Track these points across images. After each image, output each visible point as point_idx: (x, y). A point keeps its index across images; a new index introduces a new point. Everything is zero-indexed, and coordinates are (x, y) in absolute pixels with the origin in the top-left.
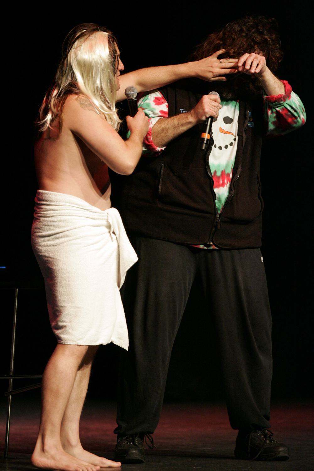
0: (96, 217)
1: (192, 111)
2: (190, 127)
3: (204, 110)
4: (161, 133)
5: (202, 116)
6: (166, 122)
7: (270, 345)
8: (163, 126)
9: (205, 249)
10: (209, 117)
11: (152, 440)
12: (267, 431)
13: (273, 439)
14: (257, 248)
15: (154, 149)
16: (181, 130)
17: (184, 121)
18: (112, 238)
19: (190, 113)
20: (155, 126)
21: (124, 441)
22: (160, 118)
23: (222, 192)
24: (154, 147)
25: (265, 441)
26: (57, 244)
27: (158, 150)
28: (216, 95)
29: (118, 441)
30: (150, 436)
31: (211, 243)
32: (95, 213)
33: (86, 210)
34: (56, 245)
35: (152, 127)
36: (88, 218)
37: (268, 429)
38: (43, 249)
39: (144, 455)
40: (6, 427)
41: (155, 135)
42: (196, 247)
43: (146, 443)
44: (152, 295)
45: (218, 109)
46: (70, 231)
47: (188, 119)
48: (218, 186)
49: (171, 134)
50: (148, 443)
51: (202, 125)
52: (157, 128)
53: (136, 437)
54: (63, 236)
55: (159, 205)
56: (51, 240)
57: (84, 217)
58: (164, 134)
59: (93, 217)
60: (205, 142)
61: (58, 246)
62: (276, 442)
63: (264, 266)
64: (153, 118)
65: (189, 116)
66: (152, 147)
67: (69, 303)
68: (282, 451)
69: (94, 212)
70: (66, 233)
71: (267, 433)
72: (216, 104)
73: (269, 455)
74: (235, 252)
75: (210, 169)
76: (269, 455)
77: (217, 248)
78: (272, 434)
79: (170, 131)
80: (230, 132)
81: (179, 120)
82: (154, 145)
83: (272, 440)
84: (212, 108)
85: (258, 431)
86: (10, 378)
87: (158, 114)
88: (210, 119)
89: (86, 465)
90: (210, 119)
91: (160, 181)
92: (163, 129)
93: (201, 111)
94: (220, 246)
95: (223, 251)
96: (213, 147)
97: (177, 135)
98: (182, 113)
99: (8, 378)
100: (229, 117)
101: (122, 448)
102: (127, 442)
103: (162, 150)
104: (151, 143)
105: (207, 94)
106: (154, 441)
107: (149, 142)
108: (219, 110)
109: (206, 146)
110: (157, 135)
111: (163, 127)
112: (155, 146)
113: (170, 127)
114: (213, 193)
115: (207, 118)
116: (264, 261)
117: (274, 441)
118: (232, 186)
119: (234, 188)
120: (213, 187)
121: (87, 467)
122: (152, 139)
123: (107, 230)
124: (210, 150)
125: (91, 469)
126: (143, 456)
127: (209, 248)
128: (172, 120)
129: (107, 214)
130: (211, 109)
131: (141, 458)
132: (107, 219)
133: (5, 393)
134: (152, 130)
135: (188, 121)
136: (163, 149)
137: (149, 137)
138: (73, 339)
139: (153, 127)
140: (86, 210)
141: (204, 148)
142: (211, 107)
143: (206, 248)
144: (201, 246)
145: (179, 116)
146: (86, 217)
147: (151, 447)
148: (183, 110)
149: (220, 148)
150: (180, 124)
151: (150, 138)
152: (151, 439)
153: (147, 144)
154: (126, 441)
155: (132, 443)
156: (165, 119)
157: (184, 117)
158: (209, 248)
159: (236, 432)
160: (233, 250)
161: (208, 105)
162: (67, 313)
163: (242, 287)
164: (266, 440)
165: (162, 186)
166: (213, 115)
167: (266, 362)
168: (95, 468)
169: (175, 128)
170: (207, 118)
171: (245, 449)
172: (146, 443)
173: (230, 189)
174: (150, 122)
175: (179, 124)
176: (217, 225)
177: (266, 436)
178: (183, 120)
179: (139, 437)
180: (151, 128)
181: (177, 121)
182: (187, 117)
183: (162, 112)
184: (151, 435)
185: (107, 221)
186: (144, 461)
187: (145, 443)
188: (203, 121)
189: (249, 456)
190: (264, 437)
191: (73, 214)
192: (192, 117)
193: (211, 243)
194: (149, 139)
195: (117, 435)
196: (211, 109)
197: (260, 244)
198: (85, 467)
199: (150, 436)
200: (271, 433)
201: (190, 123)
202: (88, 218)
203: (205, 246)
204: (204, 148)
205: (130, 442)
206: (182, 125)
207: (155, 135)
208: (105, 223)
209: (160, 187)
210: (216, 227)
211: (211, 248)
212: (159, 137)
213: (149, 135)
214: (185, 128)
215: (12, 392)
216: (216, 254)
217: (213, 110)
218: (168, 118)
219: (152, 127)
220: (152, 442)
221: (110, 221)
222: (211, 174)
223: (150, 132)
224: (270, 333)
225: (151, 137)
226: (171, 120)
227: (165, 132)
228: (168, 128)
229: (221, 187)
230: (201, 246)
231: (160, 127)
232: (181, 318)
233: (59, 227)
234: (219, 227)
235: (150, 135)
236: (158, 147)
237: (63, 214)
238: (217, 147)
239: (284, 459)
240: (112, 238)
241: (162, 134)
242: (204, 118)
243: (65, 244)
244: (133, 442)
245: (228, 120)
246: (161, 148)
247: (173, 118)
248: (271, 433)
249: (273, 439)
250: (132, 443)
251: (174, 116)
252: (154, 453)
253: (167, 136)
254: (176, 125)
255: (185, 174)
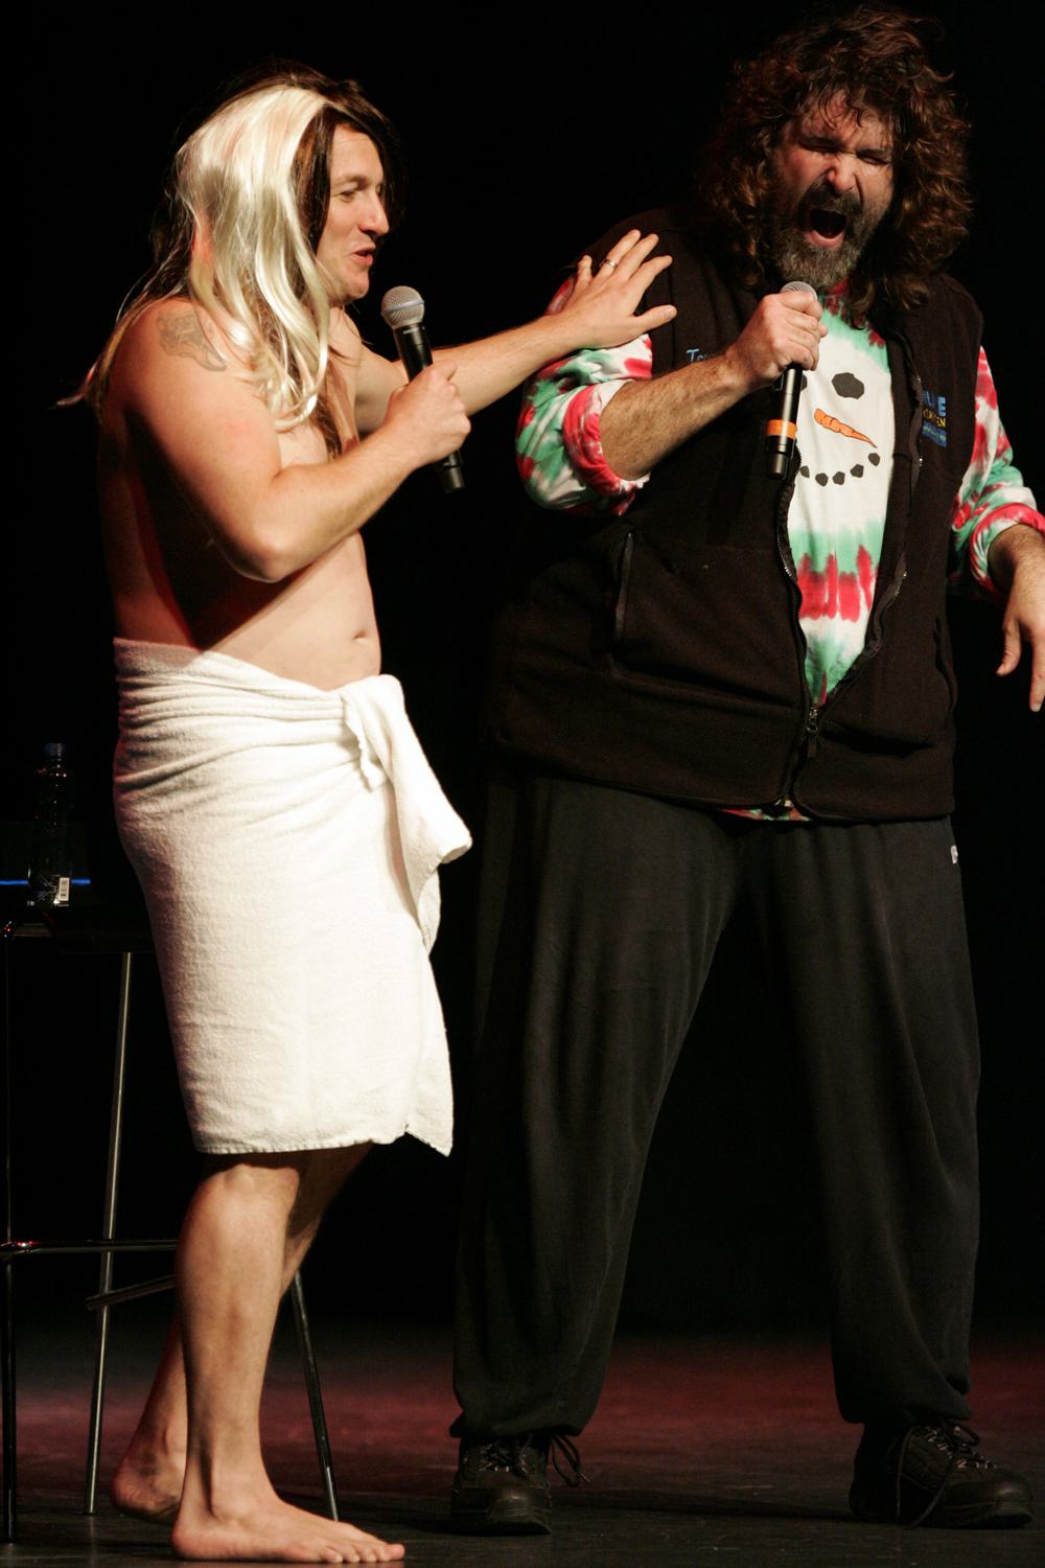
0: (296, 714)
1: (730, 352)
2: (728, 406)
3: (770, 343)
4: (631, 431)
5: (765, 364)
6: (646, 392)
7: (972, 1142)
8: (636, 405)
9: (768, 821)
10: (790, 366)
11: (574, 1457)
12: (957, 1429)
13: (977, 1455)
14: (941, 818)
15: (611, 484)
16: (696, 415)
17: (708, 389)
18: (367, 786)
19: (725, 359)
20: (612, 406)
21: (483, 1461)
22: (624, 382)
23: (839, 637)
24: (610, 478)
25: (953, 1463)
26: (163, 812)
27: (623, 490)
28: (805, 291)
29: (461, 1459)
30: (567, 1441)
31: (788, 803)
32: (290, 701)
33: (253, 691)
34: (160, 819)
35: (599, 412)
36: (265, 717)
37: (962, 1422)
38: (147, 825)
39: (548, 1508)
40: (89, 1413)
41: (612, 437)
42: (737, 816)
43: (557, 1468)
44: (587, 972)
45: (815, 337)
46: (200, 768)
47: (718, 379)
48: (819, 610)
49: (666, 431)
50: (561, 1467)
51: (767, 399)
52: (619, 412)
53: (522, 1445)
54: (180, 785)
55: (617, 674)
56: (145, 799)
57: (249, 715)
58: (643, 432)
59: (286, 714)
60: (782, 448)
61: (165, 820)
62: (990, 1465)
63: (959, 877)
64: (602, 382)
65: (722, 369)
66: (602, 477)
67: (207, 1015)
68: (1009, 1497)
69: (284, 698)
70: (187, 775)
71: (958, 1435)
72: (807, 321)
73: (964, 1509)
74: (867, 833)
75: (789, 552)
76: (964, 1509)
77: (806, 819)
78: (977, 1438)
79: (661, 420)
80: (854, 431)
81: (686, 383)
82: (610, 472)
83: (976, 1458)
84: (798, 334)
85: (928, 1428)
86: (104, 1248)
87: (618, 372)
88: (792, 373)
89: (357, 1541)
90: (792, 373)
91: (618, 593)
92: (637, 417)
93: (760, 347)
94: (812, 811)
95: (827, 831)
96: (799, 478)
97: (685, 434)
98: (695, 361)
99: (99, 1249)
100: (852, 376)
101: (477, 1487)
102: (491, 1464)
103: (635, 489)
104: (600, 466)
105: (777, 291)
106: (583, 1460)
107: (591, 461)
108: (819, 342)
109: (785, 460)
110: (618, 438)
111: (638, 408)
112: (613, 475)
113: (660, 407)
114: (799, 636)
115: (784, 371)
116: (959, 857)
117: (982, 1462)
118: (876, 623)
119: (883, 631)
120: (797, 614)
121: (360, 1546)
122: (601, 451)
123: (345, 755)
124: (789, 488)
125: (375, 1553)
126: (545, 1510)
127: (781, 818)
128: (665, 385)
129: (342, 700)
130: (795, 337)
131: (539, 1518)
132: (343, 718)
133: (88, 1299)
134: (600, 420)
135: (719, 384)
136: (640, 483)
137: (592, 444)
138: (233, 1137)
139: (604, 411)
140: (253, 691)
141: (778, 470)
142: (794, 332)
143: (767, 818)
144: (754, 812)
145: (687, 370)
146: (258, 716)
147: (573, 1479)
148: (696, 354)
149: (822, 479)
150: (693, 396)
151: (597, 449)
152: (570, 1451)
153: (587, 469)
154: (489, 1460)
155: (507, 1469)
156: (641, 384)
157: (706, 372)
158: (781, 818)
159: (860, 1428)
160: (859, 827)
161: (784, 328)
162: (203, 1046)
163: (888, 946)
164: (954, 1459)
165: (626, 610)
166: (800, 359)
167: (962, 1195)
168: (387, 1551)
169: (675, 410)
170: (784, 371)
171: (888, 1490)
172: (557, 1468)
173: (870, 635)
174: (595, 395)
175: (688, 395)
176: (806, 744)
177: (953, 1443)
178: (703, 383)
179: (531, 1445)
180: (597, 415)
181: (682, 385)
182: (715, 373)
183: (633, 364)
184: (571, 1439)
185: (344, 726)
186: (547, 1527)
187: (550, 1467)
188: (769, 380)
189: (898, 1511)
190: (949, 1449)
191: (207, 710)
192: (732, 371)
193: (788, 803)
194: (592, 453)
195: (457, 1441)
196: (795, 337)
197: (950, 805)
198: (354, 1547)
199: (567, 1441)
200: (973, 1435)
201: (726, 390)
202: (265, 717)
203: (765, 812)
204: (778, 470)
205: (503, 1466)
206: (700, 399)
207: (612, 437)
208: (335, 730)
209: (620, 614)
210: (804, 749)
211: (787, 818)
212: (626, 443)
213: (591, 439)
214: (709, 410)
215: (112, 1295)
216: (803, 839)
217: (801, 340)
218: (653, 379)
219: (599, 412)
220: (576, 1465)
221: (356, 728)
222: (793, 570)
223: (596, 429)
224: (972, 1104)
225: (599, 443)
226: (662, 386)
227: (643, 425)
228: (655, 412)
229: (824, 614)
230: (755, 814)
231: (627, 410)
232: (678, 1047)
233: (180, 755)
234: (812, 750)
235: (595, 439)
236: (622, 477)
237: (172, 713)
238: (813, 475)
239: (1015, 1522)
240: (367, 786)
241: (635, 433)
242: (772, 371)
243: (187, 814)
244: (513, 1461)
245: (848, 386)
246: (634, 482)
247: (665, 378)
248: (973, 1435)
249: (977, 1455)
250: (507, 1469)
251: (671, 372)
252: (578, 1501)
253: (650, 439)
254: (679, 400)
255: (707, 567)
